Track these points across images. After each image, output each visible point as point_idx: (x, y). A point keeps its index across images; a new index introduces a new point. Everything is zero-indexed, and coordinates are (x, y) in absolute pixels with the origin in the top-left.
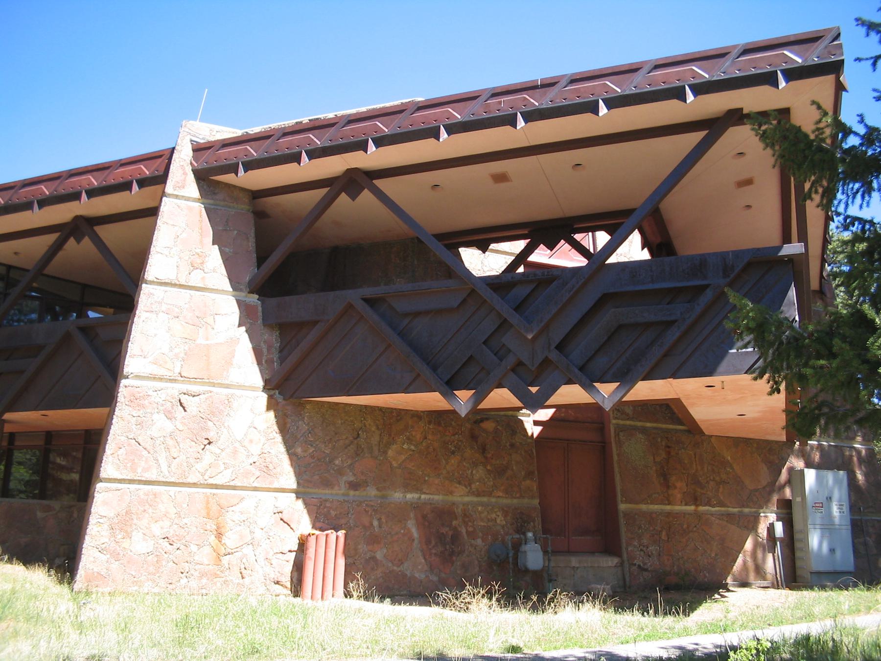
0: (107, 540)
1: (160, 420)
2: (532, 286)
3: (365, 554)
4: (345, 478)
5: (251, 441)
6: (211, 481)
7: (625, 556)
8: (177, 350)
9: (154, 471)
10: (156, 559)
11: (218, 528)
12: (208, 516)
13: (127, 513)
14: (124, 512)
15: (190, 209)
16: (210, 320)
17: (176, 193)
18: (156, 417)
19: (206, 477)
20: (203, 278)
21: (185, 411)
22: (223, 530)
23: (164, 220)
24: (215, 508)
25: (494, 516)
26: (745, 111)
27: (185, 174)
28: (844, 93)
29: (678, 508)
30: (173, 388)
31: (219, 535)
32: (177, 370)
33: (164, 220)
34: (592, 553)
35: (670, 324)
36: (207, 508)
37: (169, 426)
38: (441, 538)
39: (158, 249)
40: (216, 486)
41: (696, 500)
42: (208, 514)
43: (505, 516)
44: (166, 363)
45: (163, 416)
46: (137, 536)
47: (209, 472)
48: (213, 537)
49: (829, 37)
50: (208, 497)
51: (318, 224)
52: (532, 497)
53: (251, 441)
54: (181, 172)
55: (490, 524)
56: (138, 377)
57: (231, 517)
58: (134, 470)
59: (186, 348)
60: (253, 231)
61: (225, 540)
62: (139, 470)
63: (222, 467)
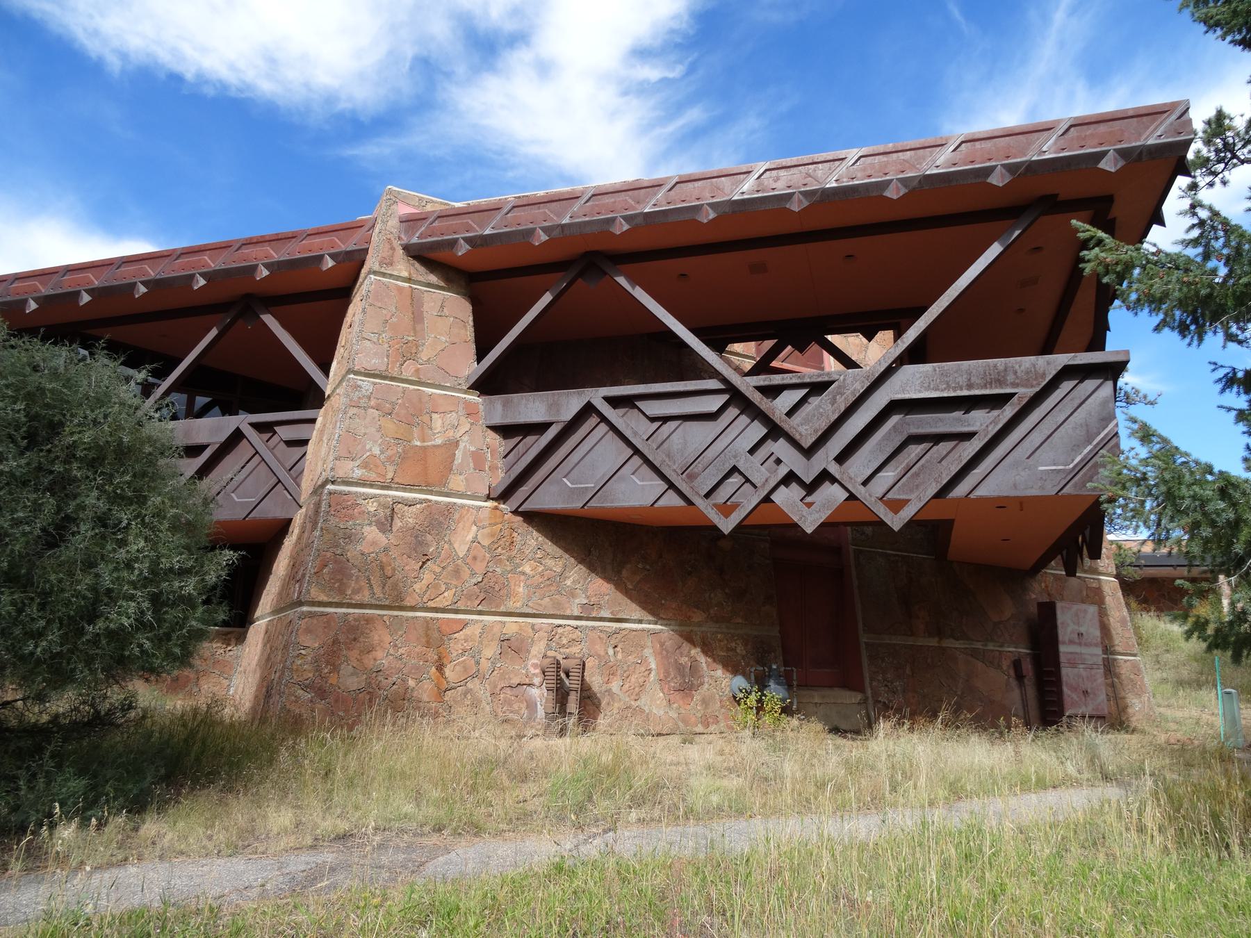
2: (804, 392)
4: (577, 601)
6: (431, 604)
7: (869, 692)
9: (367, 593)
14: (330, 642)
16: (426, 418)
17: (383, 270)
18: (367, 529)
20: (417, 370)
21: (1221, 407)
22: (445, 661)
25: (733, 645)
26: (1060, 198)
29: (921, 642)
31: (440, 668)
32: (390, 475)
34: (831, 687)
35: (969, 436)
36: (427, 635)
38: (680, 669)
40: (436, 610)
41: (939, 633)
42: (428, 642)
43: (746, 645)
45: (374, 528)
46: (346, 669)
49: (1177, 113)
50: (427, 622)
52: (1085, 612)
54: (388, 246)
55: (731, 653)
57: (455, 646)
58: (341, 591)
60: (471, 318)
61: (448, 671)
63: (443, 587)
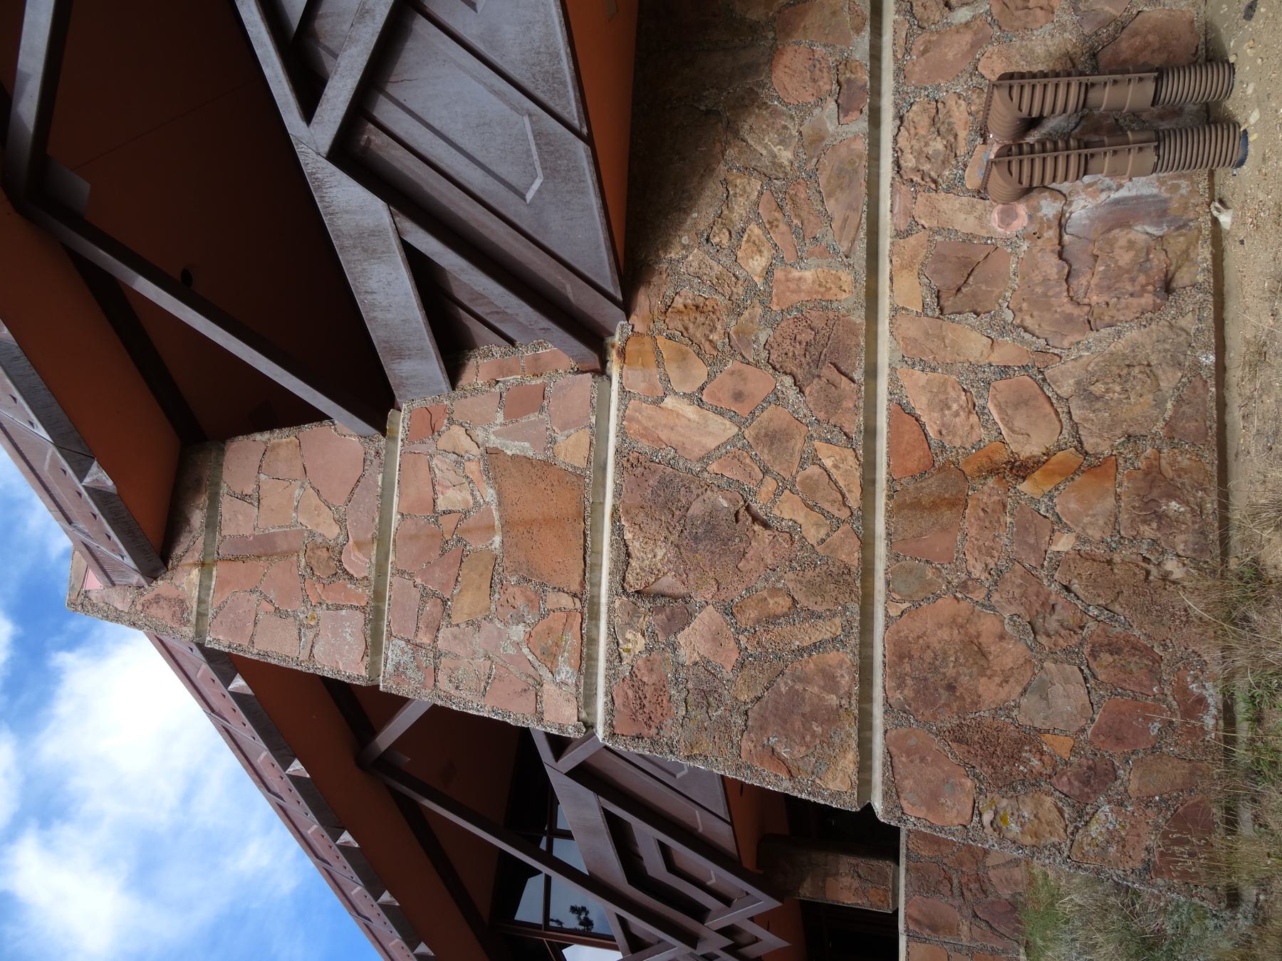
0: (1049, 801)
1: (693, 643)
3: (1063, 27)
4: (831, 127)
5: (738, 396)
6: (854, 500)
8: (520, 602)
9: (832, 657)
10: (1106, 658)
11: (994, 471)
12: (958, 503)
13: (959, 741)
14: (959, 749)
15: (222, 584)
16: (448, 523)
18: (685, 655)
19: (844, 514)
20: (359, 545)
23: (245, 643)
24: (932, 484)
27: (157, 599)
28: (381, 97)
30: (611, 610)
31: (1021, 469)
33: (245, 643)
36: (934, 506)
37: (707, 618)
39: (304, 655)
42: (952, 504)
44: (550, 631)
45: (681, 638)
46: (1031, 713)
47: (827, 506)
48: (1024, 487)
51: (371, 126)
53: (738, 396)
56: (588, 699)
59: (514, 579)
60: (258, 437)
62: (833, 700)
